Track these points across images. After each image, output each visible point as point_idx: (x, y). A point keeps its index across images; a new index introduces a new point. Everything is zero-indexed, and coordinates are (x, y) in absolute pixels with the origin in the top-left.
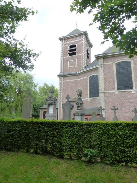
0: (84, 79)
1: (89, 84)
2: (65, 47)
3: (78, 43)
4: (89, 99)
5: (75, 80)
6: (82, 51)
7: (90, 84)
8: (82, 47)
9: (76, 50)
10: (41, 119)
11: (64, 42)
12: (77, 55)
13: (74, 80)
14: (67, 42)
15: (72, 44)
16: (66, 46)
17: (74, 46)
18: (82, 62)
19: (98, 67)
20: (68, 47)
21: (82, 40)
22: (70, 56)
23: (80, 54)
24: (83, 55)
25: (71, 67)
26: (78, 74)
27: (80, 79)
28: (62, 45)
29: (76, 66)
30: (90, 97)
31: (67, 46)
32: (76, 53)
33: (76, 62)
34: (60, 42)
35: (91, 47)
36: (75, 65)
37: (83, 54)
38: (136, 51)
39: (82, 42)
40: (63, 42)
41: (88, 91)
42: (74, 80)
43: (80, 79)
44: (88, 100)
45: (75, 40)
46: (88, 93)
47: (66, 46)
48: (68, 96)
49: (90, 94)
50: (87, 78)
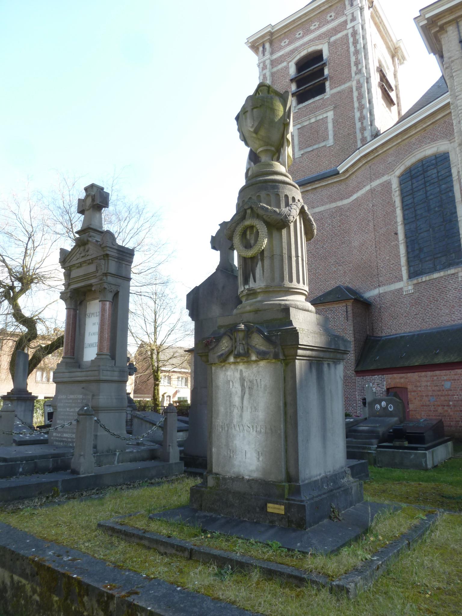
0: (372, 191)
1: (399, 212)
2: (278, 70)
3: (333, 39)
4: (405, 285)
5: (334, 205)
6: (354, 69)
7: (404, 208)
8: (352, 49)
9: (326, 72)
10: (75, 431)
11: (272, 53)
12: (330, 91)
13: (328, 206)
14: (281, 48)
15: (304, 53)
16: (280, 67)
17: (317, 57)
18: (357, 115)
19: (448, 104)
20: (287, 68)
21: (350, 17)
22: (301, 106)
23: (347, 85)
24: (358, 82)
25: (310, 149)
26: (345, 172)
27: (355, 196)
28: (264, 68)
29: (331, 142)
30: (412, 275)
31: (284, 64)
32: (327, 84)
33: (330, 126)
34: (251, 53)
35: (401, 63)
36: (326, 139)
37: (358, 77)
38: (139, 615)
39: (349, 25)
40: (267, 53)
41: (397, 246)
42: (328, 206)
43: (355, 196)
44: (401, 289)
45: (319, 27)
46: (398, 256)
47: (280, 67)
48: (86, 189)
49: (409, 262)
50: (388, 184)
